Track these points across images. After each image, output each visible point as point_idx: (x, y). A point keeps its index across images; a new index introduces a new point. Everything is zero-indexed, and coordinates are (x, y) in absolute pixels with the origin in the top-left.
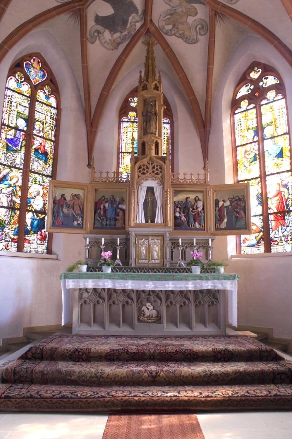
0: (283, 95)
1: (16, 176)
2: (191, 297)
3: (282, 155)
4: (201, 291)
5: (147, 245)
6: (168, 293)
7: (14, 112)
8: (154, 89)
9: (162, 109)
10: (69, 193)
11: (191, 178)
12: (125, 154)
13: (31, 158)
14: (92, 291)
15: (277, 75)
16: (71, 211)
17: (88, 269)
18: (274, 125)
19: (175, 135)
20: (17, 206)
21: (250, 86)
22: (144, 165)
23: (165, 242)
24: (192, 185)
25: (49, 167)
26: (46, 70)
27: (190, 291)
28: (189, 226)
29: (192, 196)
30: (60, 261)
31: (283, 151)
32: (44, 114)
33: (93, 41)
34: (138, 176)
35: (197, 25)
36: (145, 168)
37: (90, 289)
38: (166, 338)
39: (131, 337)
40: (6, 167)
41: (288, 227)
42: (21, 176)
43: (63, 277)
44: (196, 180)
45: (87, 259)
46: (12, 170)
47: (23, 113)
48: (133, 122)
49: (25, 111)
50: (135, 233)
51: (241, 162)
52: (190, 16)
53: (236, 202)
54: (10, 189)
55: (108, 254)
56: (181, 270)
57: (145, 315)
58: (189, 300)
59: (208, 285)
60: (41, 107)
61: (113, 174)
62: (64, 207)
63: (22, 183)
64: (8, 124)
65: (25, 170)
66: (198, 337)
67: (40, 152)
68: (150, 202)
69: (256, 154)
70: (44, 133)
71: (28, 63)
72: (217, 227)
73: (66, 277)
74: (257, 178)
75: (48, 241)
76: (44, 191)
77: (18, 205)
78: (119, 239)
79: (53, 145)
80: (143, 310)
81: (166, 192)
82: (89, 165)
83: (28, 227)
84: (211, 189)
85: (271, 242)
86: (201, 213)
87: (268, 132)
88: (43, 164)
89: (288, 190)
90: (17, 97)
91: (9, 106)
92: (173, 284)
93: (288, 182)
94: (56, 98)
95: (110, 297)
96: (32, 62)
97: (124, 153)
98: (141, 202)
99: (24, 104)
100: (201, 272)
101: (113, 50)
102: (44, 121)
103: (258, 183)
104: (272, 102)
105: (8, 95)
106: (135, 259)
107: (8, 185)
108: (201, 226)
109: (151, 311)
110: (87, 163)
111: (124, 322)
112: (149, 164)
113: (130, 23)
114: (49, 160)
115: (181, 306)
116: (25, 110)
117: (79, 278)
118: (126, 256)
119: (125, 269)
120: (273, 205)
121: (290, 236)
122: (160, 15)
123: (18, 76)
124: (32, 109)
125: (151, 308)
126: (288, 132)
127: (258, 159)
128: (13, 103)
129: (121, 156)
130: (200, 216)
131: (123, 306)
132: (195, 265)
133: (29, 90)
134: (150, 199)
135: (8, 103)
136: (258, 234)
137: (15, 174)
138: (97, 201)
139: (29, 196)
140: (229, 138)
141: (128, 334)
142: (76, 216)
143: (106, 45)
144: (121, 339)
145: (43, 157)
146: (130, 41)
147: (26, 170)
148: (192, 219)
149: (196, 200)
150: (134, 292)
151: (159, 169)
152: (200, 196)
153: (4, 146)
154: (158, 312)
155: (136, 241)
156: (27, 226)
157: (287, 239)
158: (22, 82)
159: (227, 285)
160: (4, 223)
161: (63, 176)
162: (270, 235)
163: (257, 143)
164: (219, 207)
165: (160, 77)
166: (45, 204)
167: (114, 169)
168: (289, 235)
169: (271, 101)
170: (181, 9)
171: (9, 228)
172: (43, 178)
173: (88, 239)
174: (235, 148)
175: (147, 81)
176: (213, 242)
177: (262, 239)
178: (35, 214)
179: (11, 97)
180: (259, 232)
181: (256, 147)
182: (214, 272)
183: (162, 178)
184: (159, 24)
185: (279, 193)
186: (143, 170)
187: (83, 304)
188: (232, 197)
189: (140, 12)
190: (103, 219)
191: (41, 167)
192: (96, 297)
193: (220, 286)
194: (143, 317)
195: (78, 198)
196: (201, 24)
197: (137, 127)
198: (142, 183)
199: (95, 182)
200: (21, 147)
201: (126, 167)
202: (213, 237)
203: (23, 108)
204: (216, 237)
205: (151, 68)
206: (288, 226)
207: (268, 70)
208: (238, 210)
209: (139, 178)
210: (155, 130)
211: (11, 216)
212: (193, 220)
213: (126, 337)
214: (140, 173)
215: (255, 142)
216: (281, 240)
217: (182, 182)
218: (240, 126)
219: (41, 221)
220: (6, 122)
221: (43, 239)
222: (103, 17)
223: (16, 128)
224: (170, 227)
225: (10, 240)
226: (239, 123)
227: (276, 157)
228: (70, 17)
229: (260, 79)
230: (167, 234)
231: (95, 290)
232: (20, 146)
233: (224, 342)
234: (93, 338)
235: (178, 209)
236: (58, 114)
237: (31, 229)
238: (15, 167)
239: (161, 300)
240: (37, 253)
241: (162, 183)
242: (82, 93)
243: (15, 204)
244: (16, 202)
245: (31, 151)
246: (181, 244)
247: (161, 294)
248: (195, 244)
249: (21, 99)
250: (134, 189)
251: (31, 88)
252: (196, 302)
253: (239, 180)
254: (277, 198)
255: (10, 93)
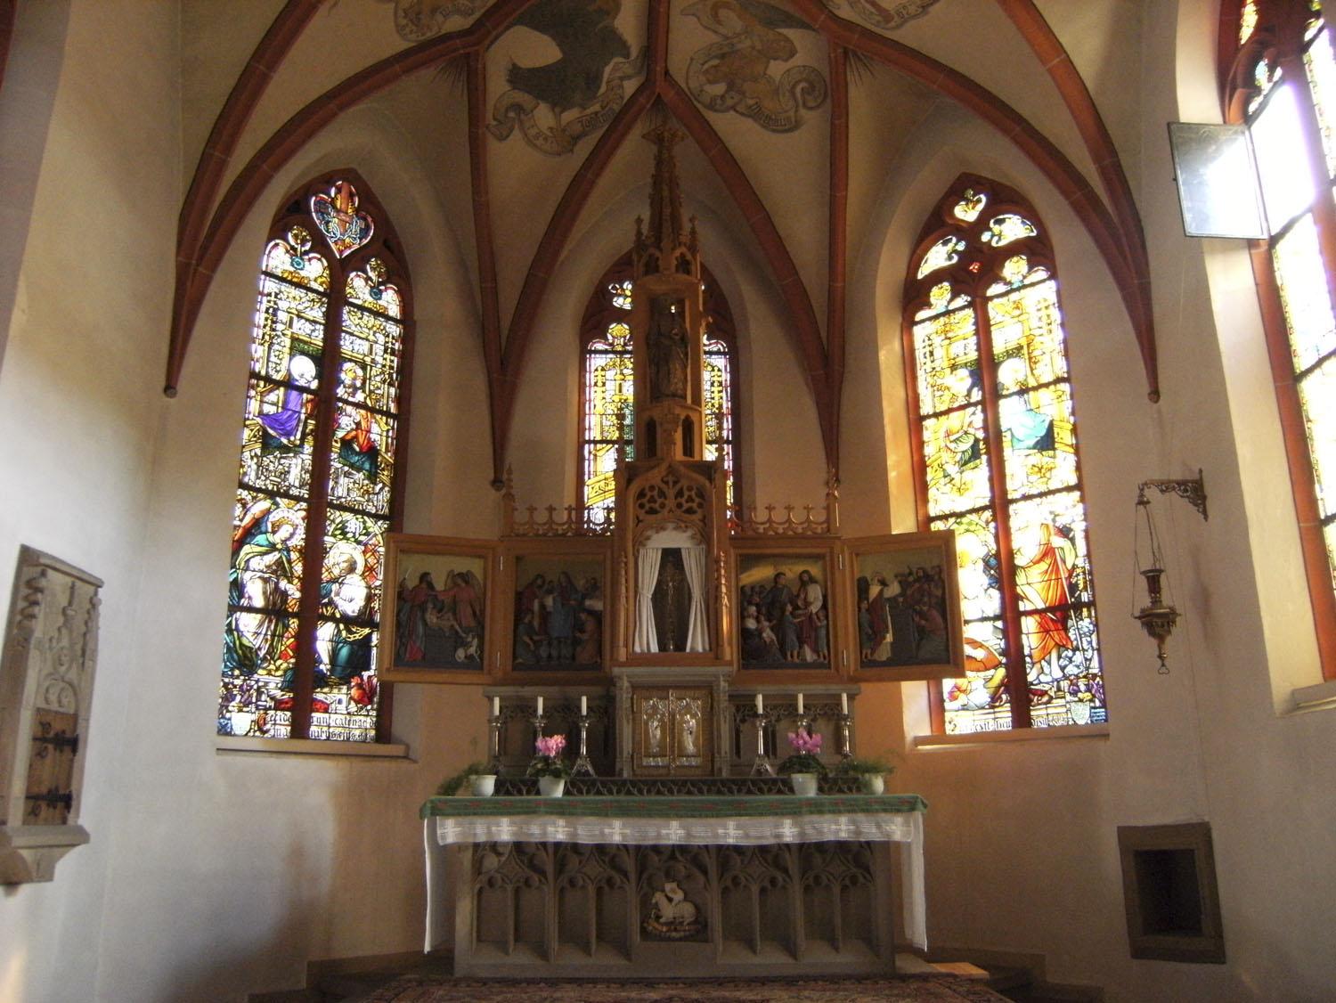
0: (1048, 269)
1: (290, 521)
2: (792, 863)
3: (1053, 442)
4: (821, 847)
5: (663, 715)
6: (725, 853)
7: (283, 338)
8: (677, 271)
9: (701, 325)
10: (440, 570)
11: (789, 520)
12: (599, 446)
13: (330, 466)
14: (511, 852)
15: (1029, 213)
16: (448, 622)
17: (499, 787)
18: (1027, 356)
19: (743, 388)
20: (293, 605)
21: (956, 244)
22: (652, 488)
23: (715, 705)
24: (790, 538)
25: (381, 489)
26: (370, 215)
27: (788, 846)
28: (785, 658)
29: (792, 571)
30: (415, 762)
31: (1056, 430)
32: (367, 340)
33: (505, 133)
34: (638, 518)
35: (794, 87)
36: (656, 497)
37: (505, 844)
38: (720, 984)
39: (623, 983)
40: (261, 496)
41: (1077, 653)
42: (303, 519)
43: (428, 812)
44: (802, 523)
45: (495, 757)
46: (277, 505)
47: (309, 340)
48: (622, 353)
49: (314, 334)
50: (630, 682)
51: (939, 462)
52: (775, 59)
53: (917, 585)
54: (271, 558)
55: (556, 742)
56: (762, 784)
57: (661, 917)
58: (786, 871)
59: (838, 827)
60: (357, 321)
61: (566, 512)
62: (429, 610)
63: (306, 540)
64: (267, 372)
65: (314, 501)
66: (815, 980)
67: (358, 449)
68: (671, 592)
69: (977, 441)
70: (367, 392)
71: (322, 199)
72: (866, 657)
73: (437, 811)
74: (983, 509)
75: (380, 704)
76: (369, 560)
77: (293, 602)
78: (584, 699)
79: (393, 428)
80: (657, 903)
81: (717, 561)
82: (497, 482)
83: (322, 667)
84: (846, 548)
85: (1032, 696)
86: (818, 618)
87: (1010, 374)
88: (366, 482)
89: (1073, 544)
90: (291, 295)
91: (269, 322)
92: (738, 827)
93: (1073, 521)
94: (400, 292)
95: (561, 867)
96: (333, 195)
97: (595, 442)
98: (645, 592)
99: (310, 314)
100: (820, 790)
101: (560, 155)
102: (366, 359)
103: (987, 523)
104: (1018, 289)
105: (266, 291)
106: (632, 756)
107: (267, 546)
108: (819, 656)
109: (681, 905)
110: (491, 476)
111: (600, 937)
112: (667, 483)
113: (608, 82)
114: (383, 469)
115: (763, 891)
116: (313, 331)
117: (475, 814)
118: (605, 745)
119: (604, 784)
120: (1035, 590)
121: (1084, 677)
122: (692, 59)
123: (296, 237)
124: (333, 326)
125: (679, 896)
126: (1066, 375)
127: (985, 453)
128: (279, 313)
129: (590, 453)
130: (816, 629)
131: (599, 891)
132: (800, 772)
133: (325, 275)
134: (670, 584)
135: (266, 315)
136: (992, 671)
137: (286, 514)
138: (519, 589)
139: (325, 576)
140: (899, 393)
141: (613, 974)
142: (464, 635)
143: (540, 142)
144: (595, 987)
145: (363, 463)
146: (607, 130)
147: (318, 505)
148: (792, 637)
149: (805, 581)
150: (628, 853)
151: (694, 496)
152: (815, 570)
153: (255, 436)
154: (697, 907)
155: (632, 703)
156: (321, 662)
157: (1075, 688)
158: (306, 253)
159: (894, 827)
160: (254, 656)
161: (425, 520)
162: (1026, 674)
163: (980, 407)
164: (871, 600)
165: (693, 232)
166: (369, 598)
167: (570, 500)
168: (1081, 675)
169: (1015, 286)
170: (748, 43)
171: (270, 670)
172: (364, 522)
173: (497, 701)
174: (916, 422)
175: (658, 246)
176: (856, 702)
177: (1003, 688)
178: (342, 626)
179: (276, 297)
180: (996, 667)
181: (978, 419)
182: (859, 790)
183: (705, 524)
184: (690, 81)
185: (1048, 552)
186: (649, 502)
187: (486, 886)
188: (907, 571)
189: (634, 52)
190: (541, 641)
191: (359, 490)
192: (523, 867)
193: (874, 830)
194: (656, 925)
195: (467, 582)
196: (806, 80)
197: (631, 366)
198: (648, 538)
199: (517, 535)
200: (304, 436)
201: (602, 484)
202: (853, 687)
203: (308, 327)
204: (864, 686)
205: (667, 211)
206: (1077, 649)
207: (1003, 200)
208: (925, 608)
209: (640, 524)
210: (682, 387)
211: (273, 635)
212: (795, 639)
213: (608, 981)
214: (643, 511)
215: (975, 404)
216: (1059, 689)
217: (761, 531)
218: (928, 360)
219: (359, 646)
220: (259, 367)
221: (366, 699)
222: (530, 70)
223: (289, 384)
224: (730, 663)
225: (273, 704)
226: (928, 349)
227: (1034, 448)
228: (439, 72)
229: (982, 223)
230: (722, 684)
231: (518, 847)
232: (299, 435)
233: (887, 992)
234: (514, 987)
235: (753, 609)
236: (406, 338)
237: (332, 671)
238: (286, 495)
239: (705, 872)
240: (348, 739)
241: (704, 537)
242: (474, 276)
243: (287, 599)
244: (288, 595)
245: (332, 446)
246: (761, 711)
247: (706, 854)
248: (801, 710)
249: (303, 300)
250: (626, 557)
251: (330, 267)
252: (807, 879)
253: (932, 514)
254: (1044, 566)
255: (270, 286)
